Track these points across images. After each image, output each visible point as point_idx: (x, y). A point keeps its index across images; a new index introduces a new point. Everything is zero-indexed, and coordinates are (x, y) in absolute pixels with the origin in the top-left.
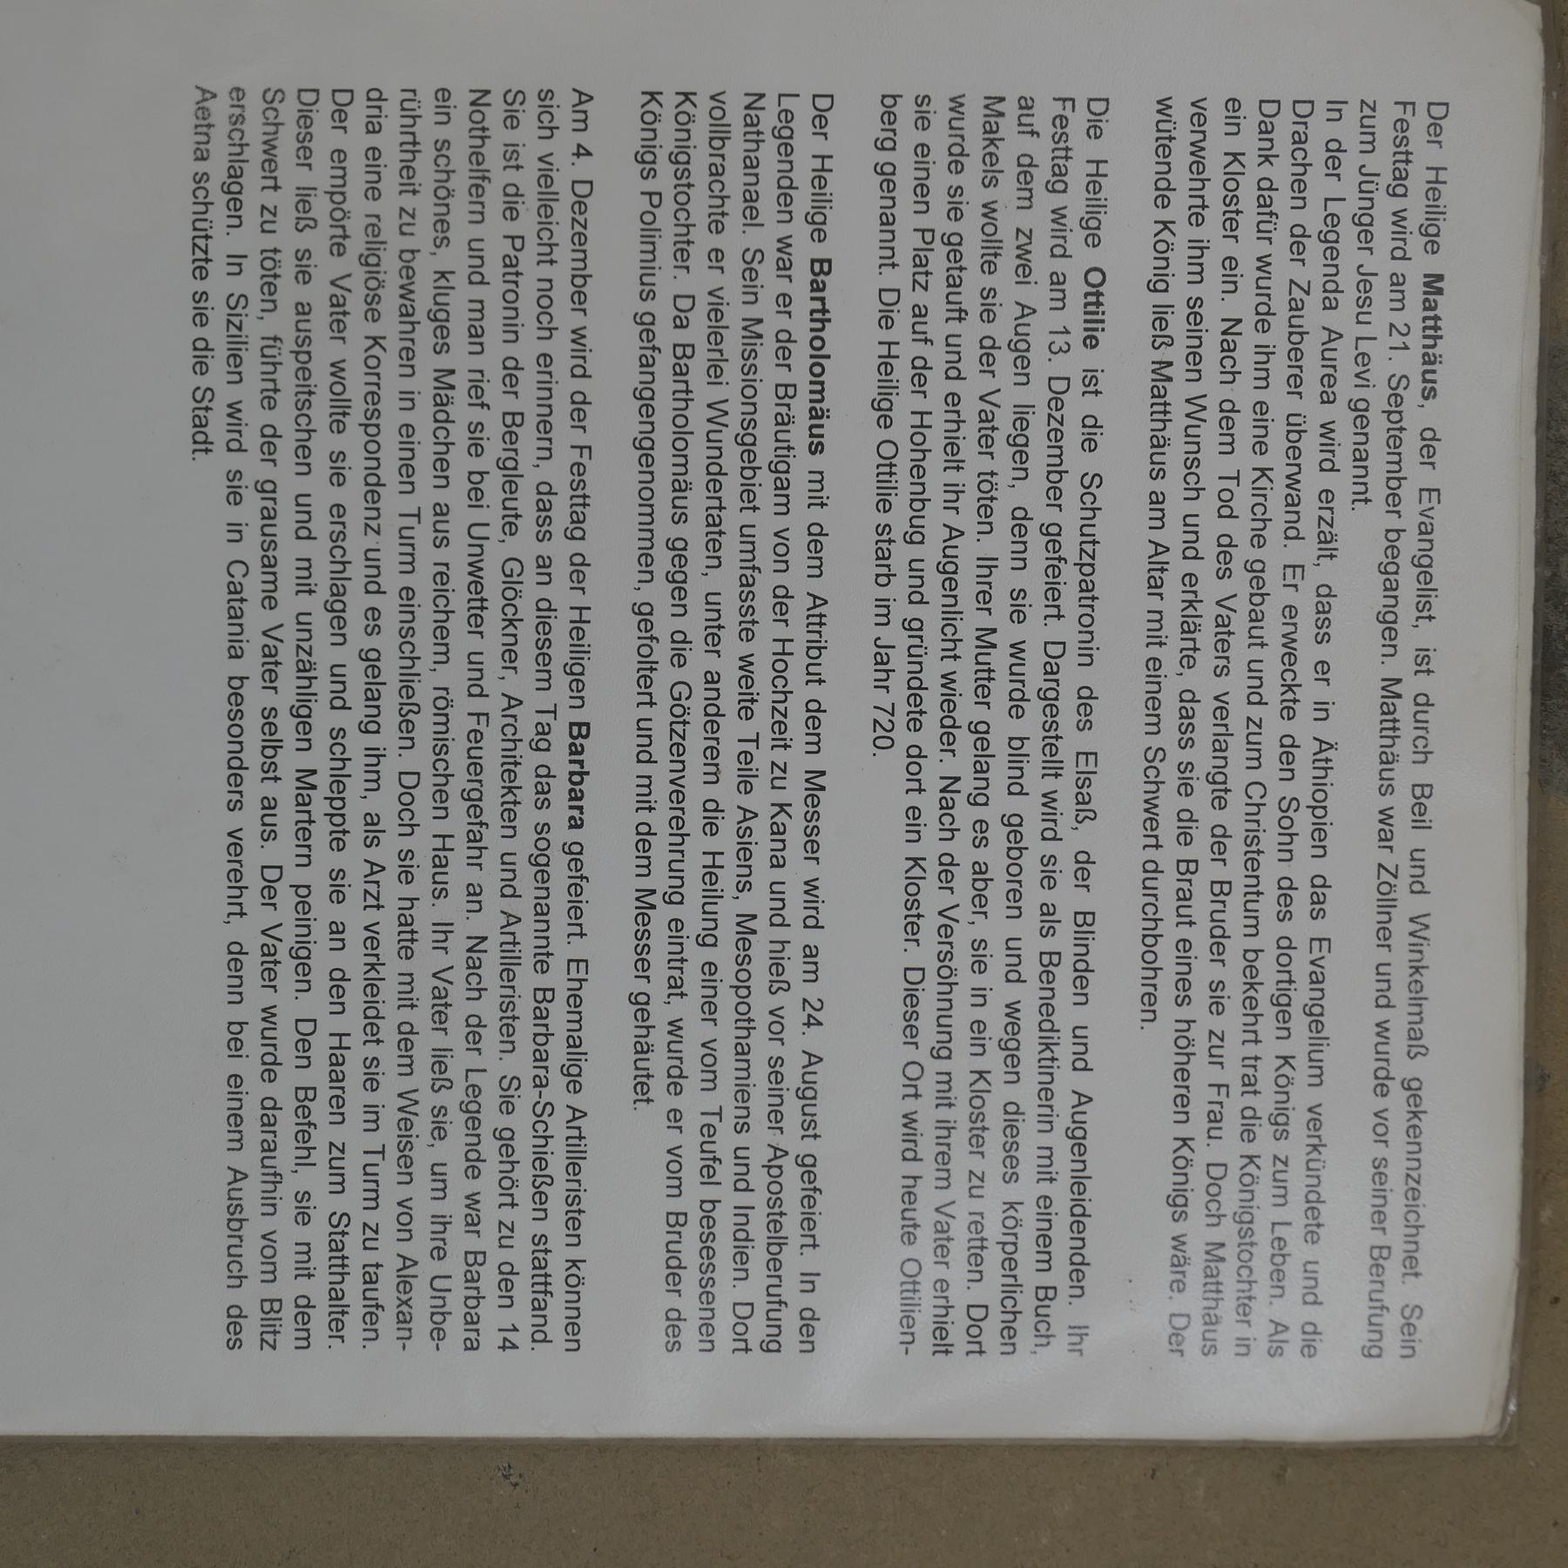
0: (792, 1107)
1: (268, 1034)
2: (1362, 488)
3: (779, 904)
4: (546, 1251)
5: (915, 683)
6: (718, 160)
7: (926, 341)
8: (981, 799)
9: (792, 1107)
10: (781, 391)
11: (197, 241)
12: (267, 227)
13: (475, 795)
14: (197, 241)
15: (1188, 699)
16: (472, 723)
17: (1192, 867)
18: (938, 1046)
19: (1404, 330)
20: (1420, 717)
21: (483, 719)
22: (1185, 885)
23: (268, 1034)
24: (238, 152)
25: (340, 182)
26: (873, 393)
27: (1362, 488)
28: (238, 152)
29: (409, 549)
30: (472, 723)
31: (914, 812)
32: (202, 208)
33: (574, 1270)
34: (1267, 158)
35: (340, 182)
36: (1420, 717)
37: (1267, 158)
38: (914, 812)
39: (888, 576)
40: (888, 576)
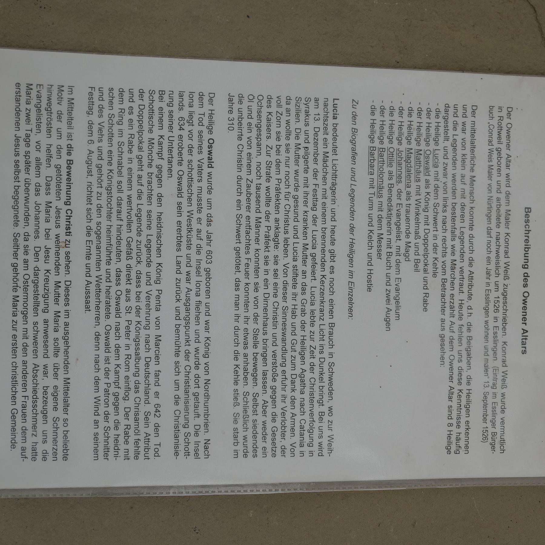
1: (196, 355)
3: (250, 112)
5: (408, 232)
6: (150, 179)
8: (311, 445)
10: (331, 325)
12: (99, 198)
13: (446, 118)
15: (139, 273)
16: (246, 261)
17: (333, 325)
20: (471, 240)
21: (249, 260)
22: (331, 330)
23: (196, 355)
26: (446, 444)
30: (246, 261)
31: (239, 201)
33: (247, 286)
34: (293, 390)
36: (471, 240)
37: (293, 390)
38: (239, 201)
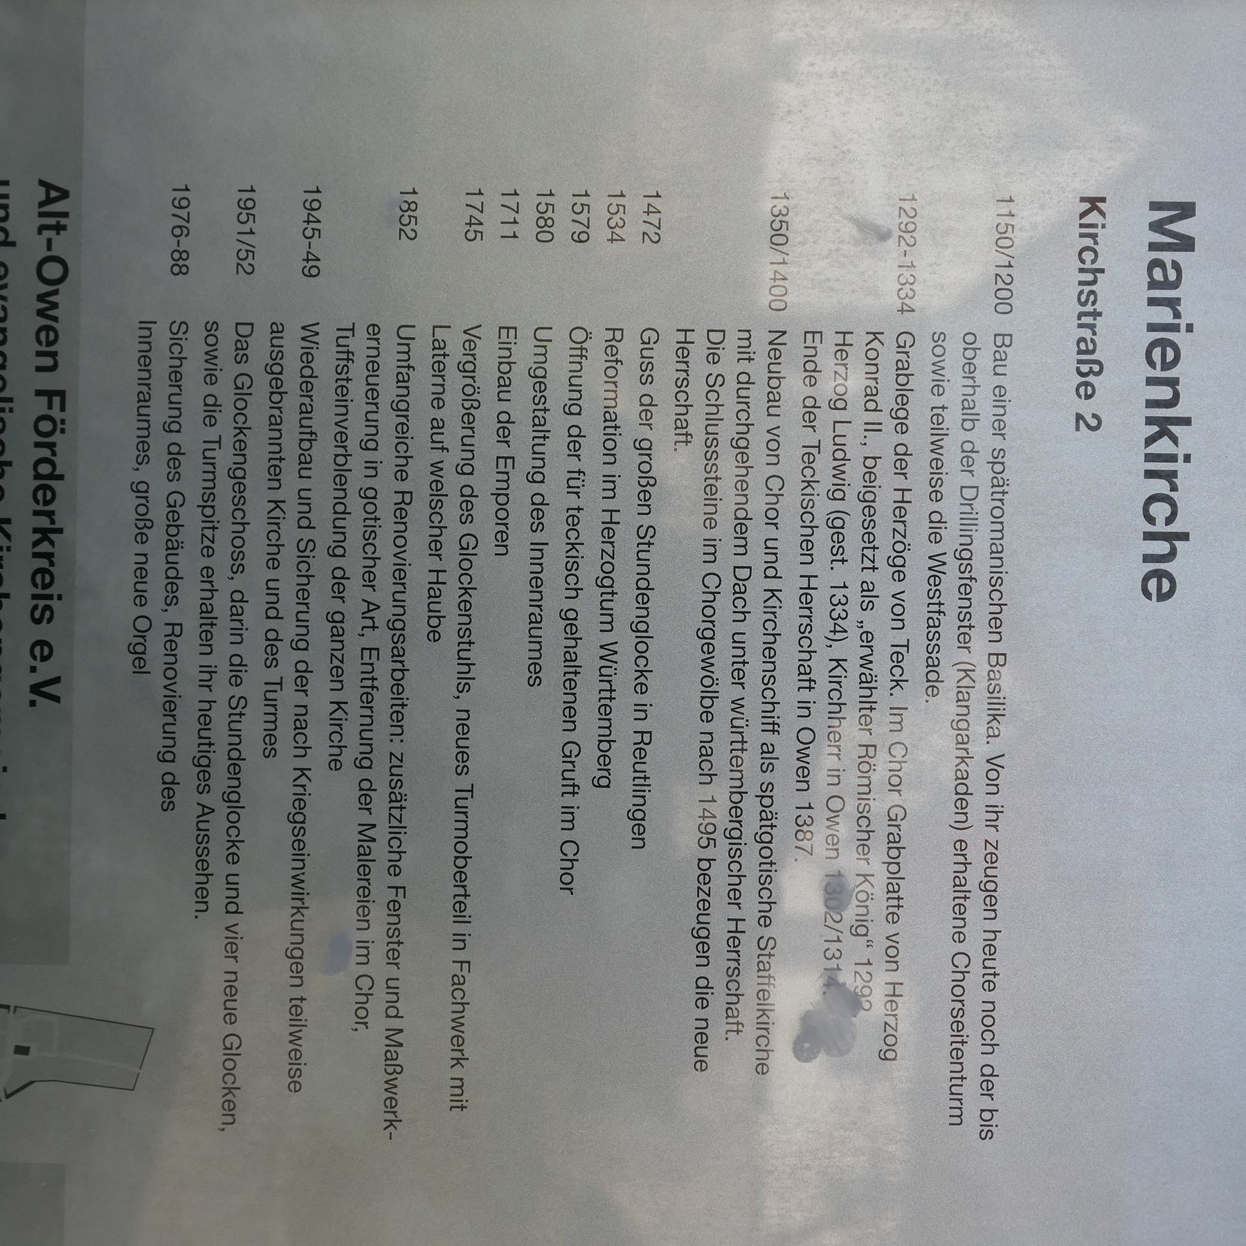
0: (158, 512)
2: (277, 448)
4: (545, 410)
7: (443, 449)
9: (158, 512)
11: (866, 552)
14: (866, 552)
16: (391, 894)
18: (737, 437)
19: (1094, 423)
24: (1193, 250)
25: (504, 485)
27: (277, 448)
28: (1193, 250)
29: (272, 710)
30: (391, 894)
32: (770, 707)
35: (504, 485)
39: (345, 456)
40: (345, 456)
